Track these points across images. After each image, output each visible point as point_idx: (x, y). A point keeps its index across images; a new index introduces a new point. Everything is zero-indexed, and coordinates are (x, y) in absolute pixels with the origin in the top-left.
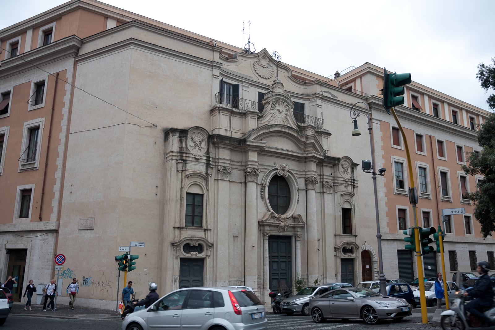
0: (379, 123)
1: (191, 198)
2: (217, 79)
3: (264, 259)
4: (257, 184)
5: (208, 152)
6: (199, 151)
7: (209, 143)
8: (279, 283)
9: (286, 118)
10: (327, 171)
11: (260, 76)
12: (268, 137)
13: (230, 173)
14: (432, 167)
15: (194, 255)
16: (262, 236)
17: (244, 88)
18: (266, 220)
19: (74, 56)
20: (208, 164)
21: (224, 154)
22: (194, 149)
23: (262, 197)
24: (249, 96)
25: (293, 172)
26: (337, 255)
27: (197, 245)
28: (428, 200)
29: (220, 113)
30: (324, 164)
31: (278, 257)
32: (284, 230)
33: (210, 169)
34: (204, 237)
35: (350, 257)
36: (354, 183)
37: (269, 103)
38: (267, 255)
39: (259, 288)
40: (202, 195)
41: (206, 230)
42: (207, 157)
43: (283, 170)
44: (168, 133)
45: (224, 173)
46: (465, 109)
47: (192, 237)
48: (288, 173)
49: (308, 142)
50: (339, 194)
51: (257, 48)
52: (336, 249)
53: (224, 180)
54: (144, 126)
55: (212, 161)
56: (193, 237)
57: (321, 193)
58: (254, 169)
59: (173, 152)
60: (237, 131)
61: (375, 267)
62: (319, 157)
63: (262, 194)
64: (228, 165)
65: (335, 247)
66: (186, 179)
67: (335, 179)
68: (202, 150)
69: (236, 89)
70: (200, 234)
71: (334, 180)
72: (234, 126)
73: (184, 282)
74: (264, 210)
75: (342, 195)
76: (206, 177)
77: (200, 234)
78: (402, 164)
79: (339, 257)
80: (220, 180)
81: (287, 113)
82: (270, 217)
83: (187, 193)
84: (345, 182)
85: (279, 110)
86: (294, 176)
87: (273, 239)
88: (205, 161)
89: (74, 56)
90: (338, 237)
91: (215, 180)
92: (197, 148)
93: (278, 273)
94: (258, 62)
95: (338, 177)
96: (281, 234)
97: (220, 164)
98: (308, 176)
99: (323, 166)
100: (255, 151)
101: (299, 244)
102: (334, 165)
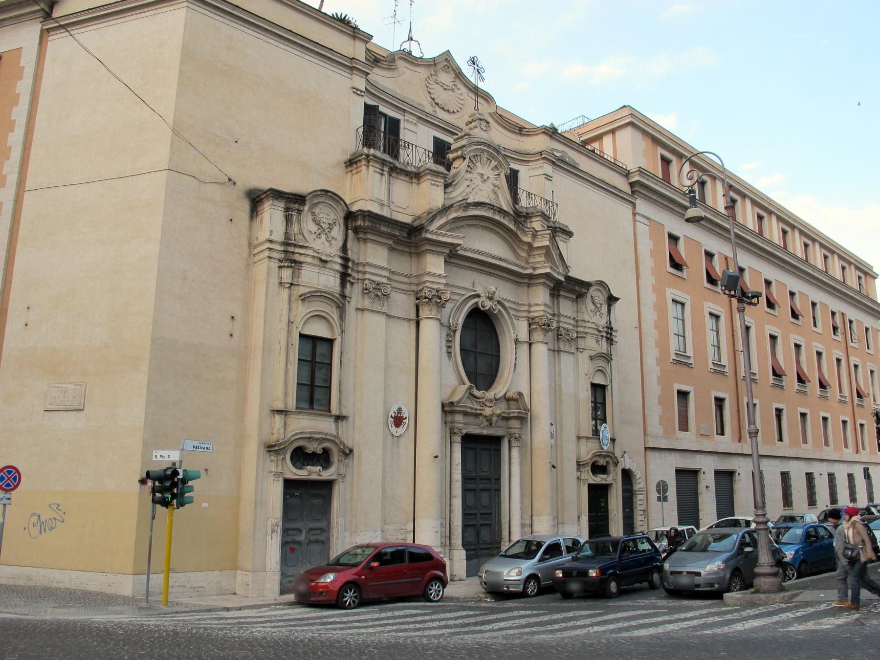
0: (647, 223)
1: (308, 346)
2: (360, 98)
3: (453, 483)
4: (441, 324)
5: (344, 248)
6: (327, 244)
7: (347, 229)
8: (478, 534)
9: (495, 193)
10: (566, 307)
11: (437, 104)
12: (476, 226)
13: (387, 296)
14: (728, 314)
15: (312, 473)
16: (448, 436)
17: (408, 126)
18: (459, 402)
19: (41, 19)
20: (344, 277)
21: (375, 256)
22: (317, 240)
23: (449, 353)
24: (418, 140)
25: (507, 305)
26: (582, 477)
27: (319, 451)
28: (722, 376)
29: (368, 167)
30: (562, 293)
31: (475, 479)
32: (491, 424)
33: (348, 285)
34: (334, 433)
35: (604, 482)
36: (611, 334)
37: (464, 159)
38: (458, 475)
39: (443, 545)
40: (330, 342)
41: (339, 418)
42: (342, 258)
43: (491, 299)
44: (256, 199)
45: (377, 295)
46: (775, 213)
47: (311, 433)
48: (499, 307)
49: (536, 245)
50: (587, 354)
51: (429, 50)
52: (579, 465)
53: (378, 312)
54: (208, 180)
55: (352, 269)
56: (314, 433)
57: (554, 351)
58: (437, 291)
59: (271, 241)
60: (401, 210)
61: (640, 502)
62: (556, 275)
63: (449, 347)
64: (385, 280)
65: (578, 462)
66: (300, 302)
67: (580, 324)
68: (333, 242)
69: (394, 126)
70: (324, 425)
71: (577, 326)
72: (395, 197)
73: (290, 532)
74: (451, 379)
75: (592, 358)
76: (341, 302)
77: (324, 425)
78: (683, 304)
79: (585, 481)
80: (368, 310)
81: (495, 182)
82: (467, 395)
83: (302, 336)
84: (597, 333)
85: (482, 175)
86: (508, 313)
87: (469, 440)
88: (338, 267)
89: (41, 19)
90: (583, 441)
91: (357, 309)
92: (323, 237)
93: (475, 514)
94: (434, 77)
95: (585, 321)
96: (485, 432)
97: (367, 276)
98: (535, 314)
99: (558, 296)
100: (439, 253)
101: (515, 453)
102: (577, 297)
